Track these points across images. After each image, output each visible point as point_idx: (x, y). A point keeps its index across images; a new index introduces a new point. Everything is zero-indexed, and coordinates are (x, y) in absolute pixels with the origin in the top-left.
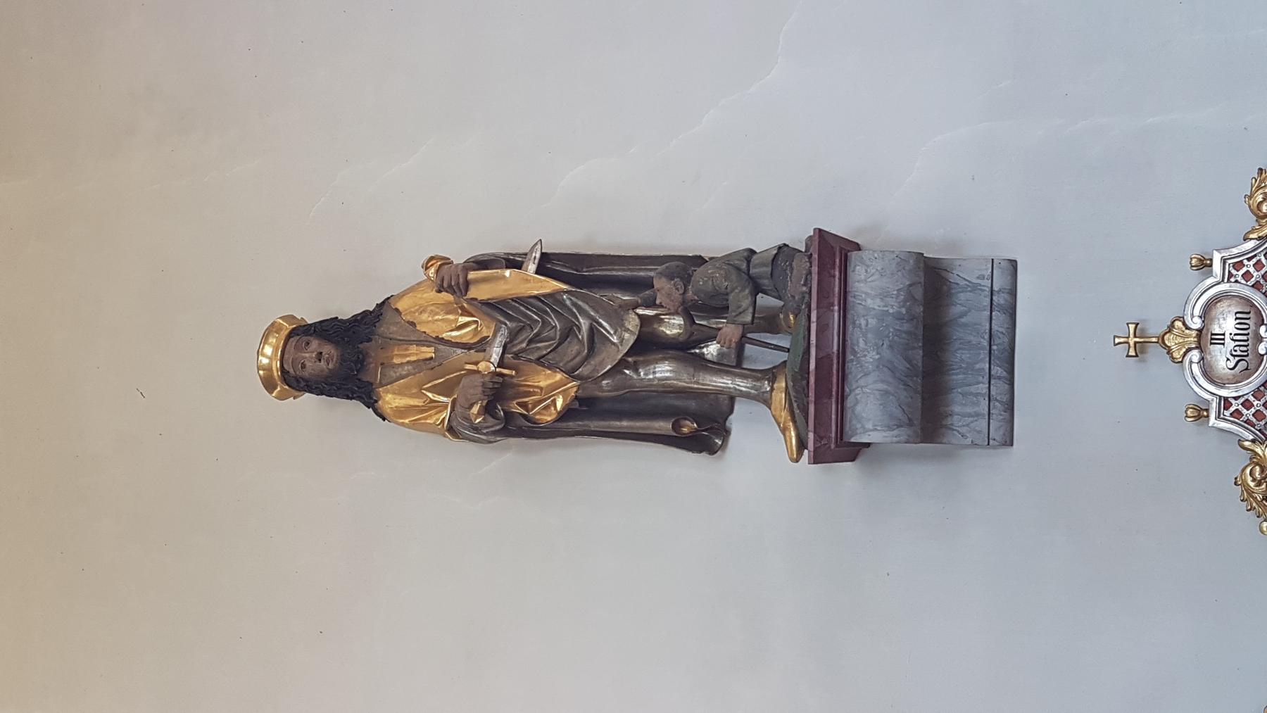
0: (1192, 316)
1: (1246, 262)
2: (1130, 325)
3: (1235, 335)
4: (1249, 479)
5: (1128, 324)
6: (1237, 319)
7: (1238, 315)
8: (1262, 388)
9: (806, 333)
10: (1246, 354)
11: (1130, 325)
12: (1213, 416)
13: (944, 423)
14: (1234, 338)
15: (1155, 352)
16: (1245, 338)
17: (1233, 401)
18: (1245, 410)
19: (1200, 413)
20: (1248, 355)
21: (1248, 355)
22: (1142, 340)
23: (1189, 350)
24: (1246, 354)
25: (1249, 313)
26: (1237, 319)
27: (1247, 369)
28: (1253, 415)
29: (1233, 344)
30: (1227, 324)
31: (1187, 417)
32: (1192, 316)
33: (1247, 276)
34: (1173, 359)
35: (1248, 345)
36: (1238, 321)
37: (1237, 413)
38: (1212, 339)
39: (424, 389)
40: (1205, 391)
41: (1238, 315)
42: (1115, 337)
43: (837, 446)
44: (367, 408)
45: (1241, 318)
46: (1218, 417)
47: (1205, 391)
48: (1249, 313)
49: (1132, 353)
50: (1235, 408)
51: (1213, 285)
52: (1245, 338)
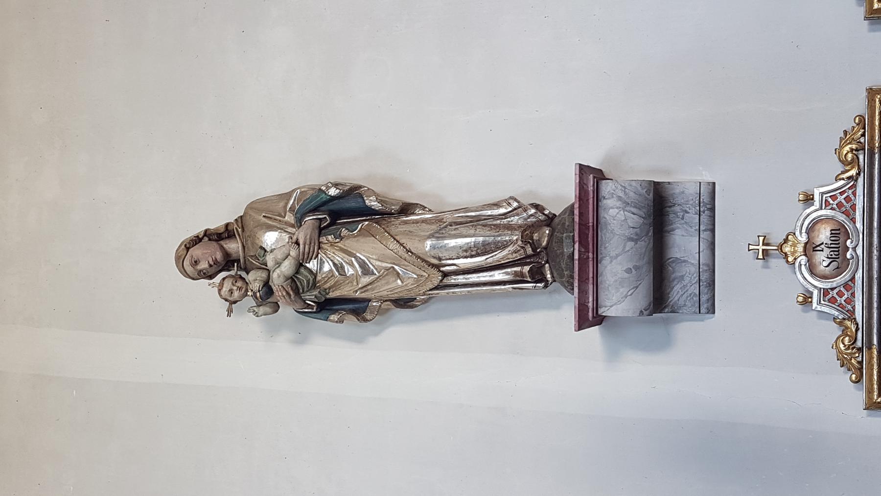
0: (801, 233)
2: (750, 249)
3: (831, 244)
4: (842, 346)
5: (749, 250)
6: (831, 234)
8: (850, 283)
10: (837, 257)
11: (750, 249)
14: (829, 246)
15: (777, 263)
24: (837, 257)
28: (844, 301)
32: (801, 233)
33: (840, 205)
34: (787, 262)
36: (831, 235)
38: (838, 251)
41: (833, 232)
43: (593, 317)
45: (835, 233)
48: (839, 230)
49: (761, 256)
51: (815, 211)
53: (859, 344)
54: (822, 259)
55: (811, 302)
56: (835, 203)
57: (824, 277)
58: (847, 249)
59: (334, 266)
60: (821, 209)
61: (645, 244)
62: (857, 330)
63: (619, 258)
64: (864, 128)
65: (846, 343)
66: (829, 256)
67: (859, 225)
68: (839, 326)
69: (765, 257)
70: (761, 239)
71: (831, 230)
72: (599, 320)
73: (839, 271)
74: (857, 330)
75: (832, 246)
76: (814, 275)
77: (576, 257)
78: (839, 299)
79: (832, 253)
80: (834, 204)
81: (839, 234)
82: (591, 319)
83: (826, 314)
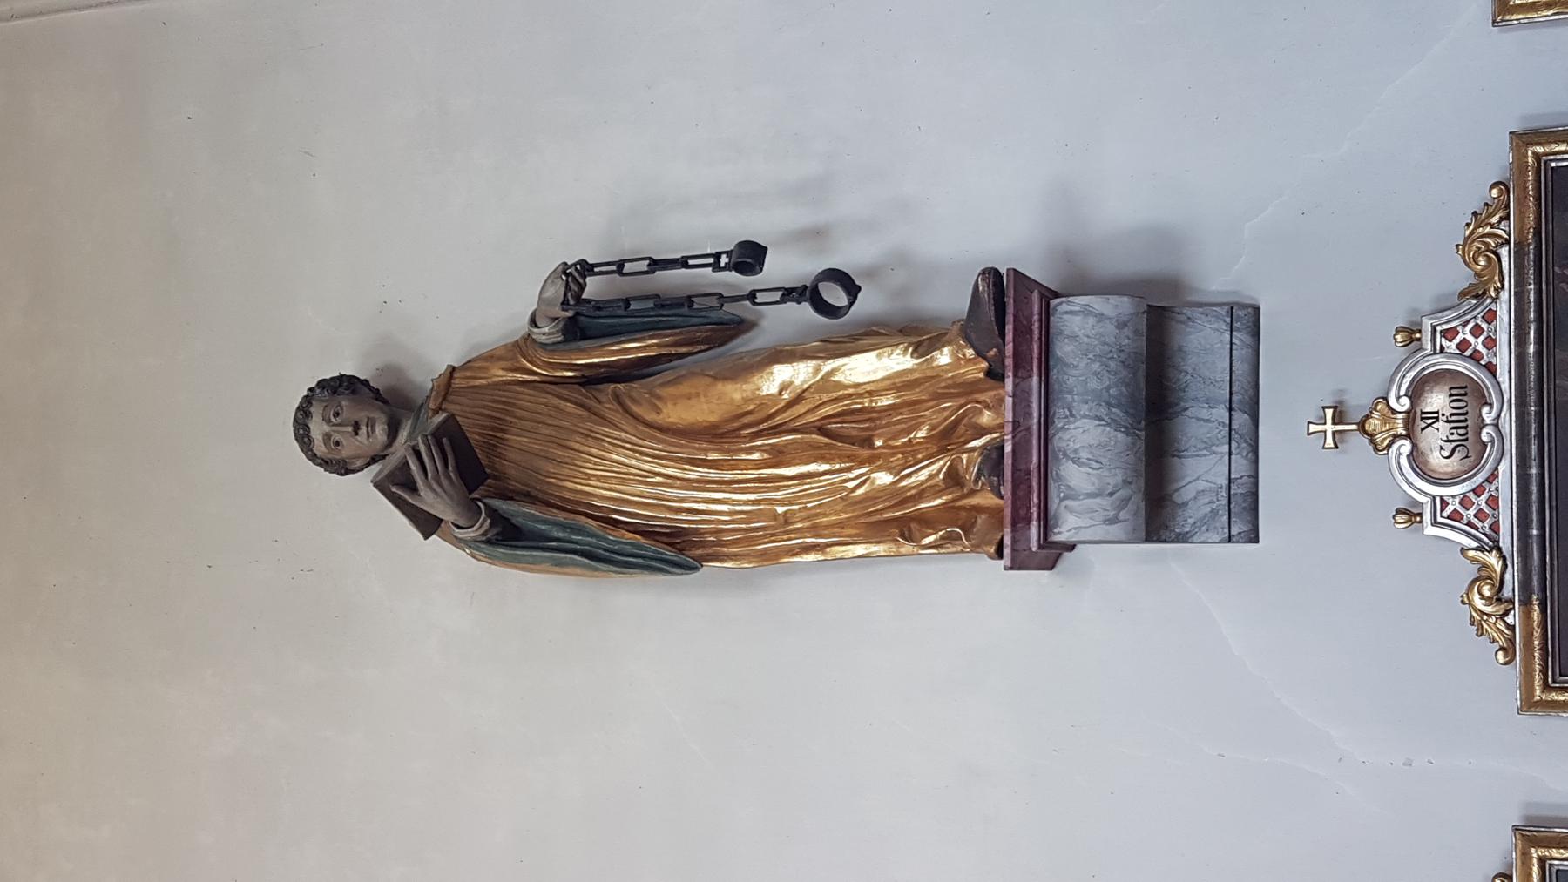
1: (1460, 329)
2: (1311, 431)
3: (1452, 415)
5: (1309, 434)
6: (1451, 395)
7: (1454, 392)
9: (552, 428)
10: (1463, 438)
11: (1311, 431)
12: (1427, 517)
13: (1179, 501)
14: (1450, 419)
16: (1462, 418)
17: (1450, 501)
18: (1458, 509)
19: (1411, 514)
20: (1467, 440)
21: (1467, 440)
22: (928, 336)
23: (1396, 437)
24: (1463, 438)
25: (1466, 387)
26: (1451, 395)
27: (1467, 457)
28: (1475, 516)
29: (1448, 426)
30: (1437, 400)
31: (1395, 522)
33: (1463, 345)
35: (1467, 434)
37: (1455, 516)
38: (1465, 427)
39: (484, 504)
40: (1422, 491)
41: (1454, 392)
42: (1309, 423)
43: (1040, 547)
44: (417, 535)
46: (1435, 523)
47: (1422, 491)
49: (1330, 442)
50: (1464, 514)
52: (1462, 418)
53: (1507, 593)
54: (1435, 438)
55: (1421, 522)
56: (1466, 336)
57: (1455, 479)
58: (1482, 425)
59: (400, 495)
60: (1435, 353)
61: (1050, 390)
62: (1505, 567)
63: (1133, 499)
64: (1507, 206)
65: (1487, 593)
66: (1451, 438)
67: (1503, 376)
68: (1125, 436)
69: (1339, 445)
70: (1329, 413)
71: (1451, 389)
72: (1255, 308)
73: (1476, 465)
74: (1505, 567)
75: (1454, 418)
76: (564, 381)
77: (1008, 448)
78: (1458, 507)
79: (1454, 431)
80: (1452, 346)
81: (1465, 395)
82: (1034, 549)
83: (1448, 543)
